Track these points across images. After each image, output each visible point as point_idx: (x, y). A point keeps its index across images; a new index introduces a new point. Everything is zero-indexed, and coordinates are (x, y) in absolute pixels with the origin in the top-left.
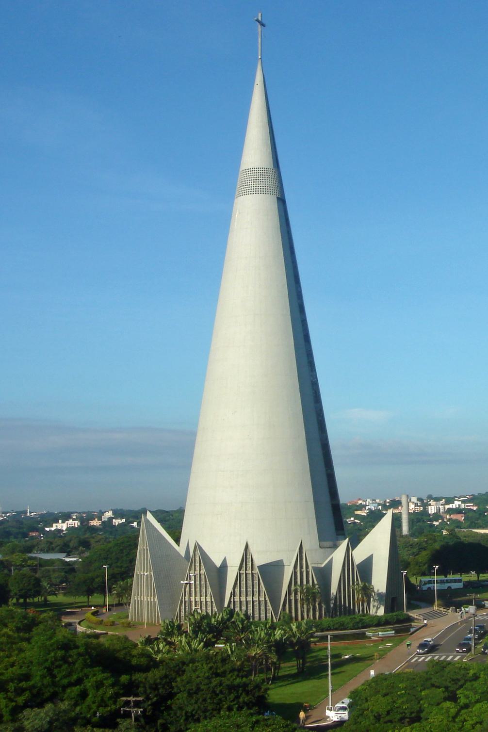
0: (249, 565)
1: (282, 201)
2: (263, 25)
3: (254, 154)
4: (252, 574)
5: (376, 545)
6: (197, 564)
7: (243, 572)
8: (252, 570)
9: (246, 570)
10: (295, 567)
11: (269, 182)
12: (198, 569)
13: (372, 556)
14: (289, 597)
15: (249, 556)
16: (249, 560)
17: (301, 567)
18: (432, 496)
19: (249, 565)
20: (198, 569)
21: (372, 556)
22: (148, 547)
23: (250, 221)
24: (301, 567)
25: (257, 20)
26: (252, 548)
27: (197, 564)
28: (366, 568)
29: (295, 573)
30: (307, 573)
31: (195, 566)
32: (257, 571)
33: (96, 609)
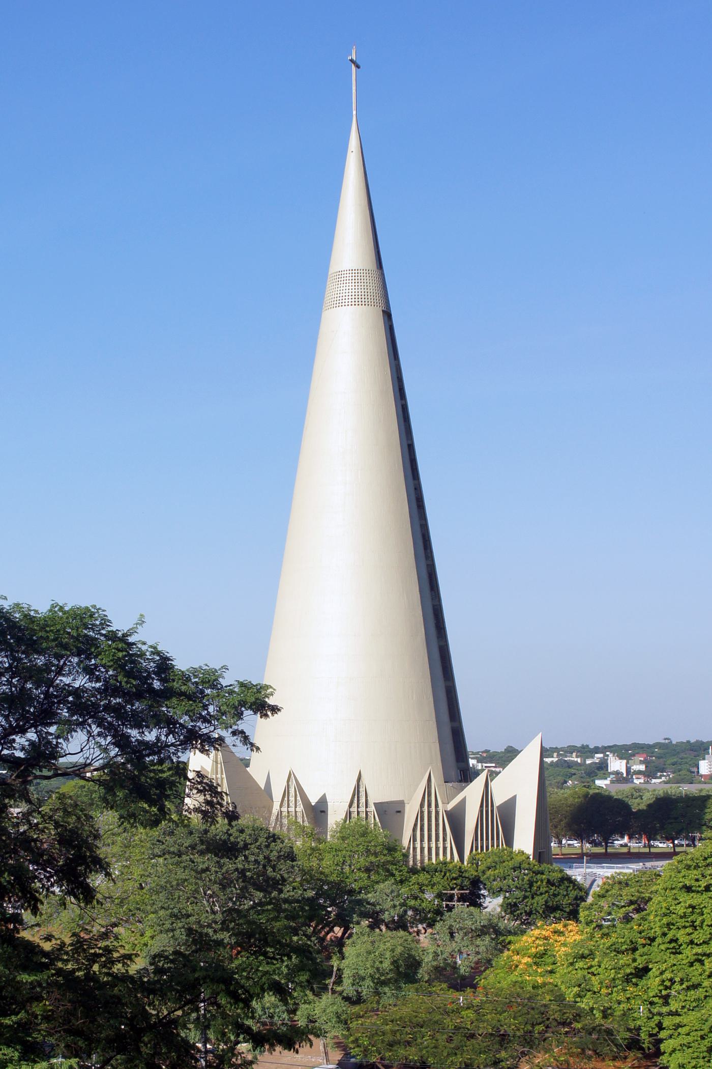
0: (363, 800)
1: (387, 315)
2: (358, 67)
3: (349, 249)
4: (367, 812)
5: (519, 785)
6: (292, 799)
7: (354, 809)
8: (366, 807)
9: (358, 807)
10: (422, 805)
11: (371, 286)
12: (292, 804)
13: (515, 797)
14: (414, 844)
15: (362, 790)
16: (363, 794)
17: (429, 805)
18: (587, 746)
19: (363, 800)
20: (292, 804)
21: (515, 797)
22: (224, 776)
23: (345, 339)
24: (429, 805)
25: (352, 60)
26: (365, 780)
27: (292, 799)
28: (507, 813)
29: (422, 812)
30: (437, 813)
31: (288, 800)
32: (372, 808)
33: (661, 751)
